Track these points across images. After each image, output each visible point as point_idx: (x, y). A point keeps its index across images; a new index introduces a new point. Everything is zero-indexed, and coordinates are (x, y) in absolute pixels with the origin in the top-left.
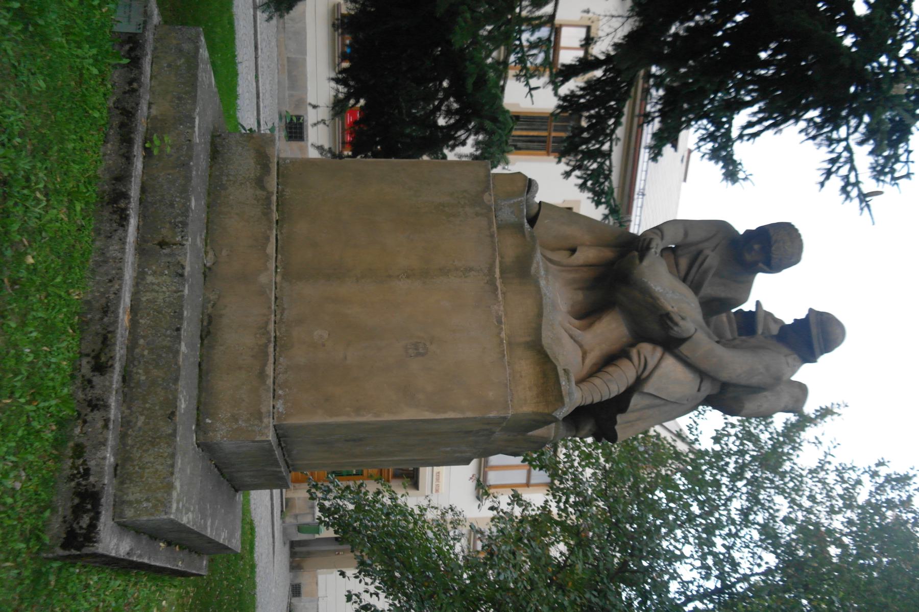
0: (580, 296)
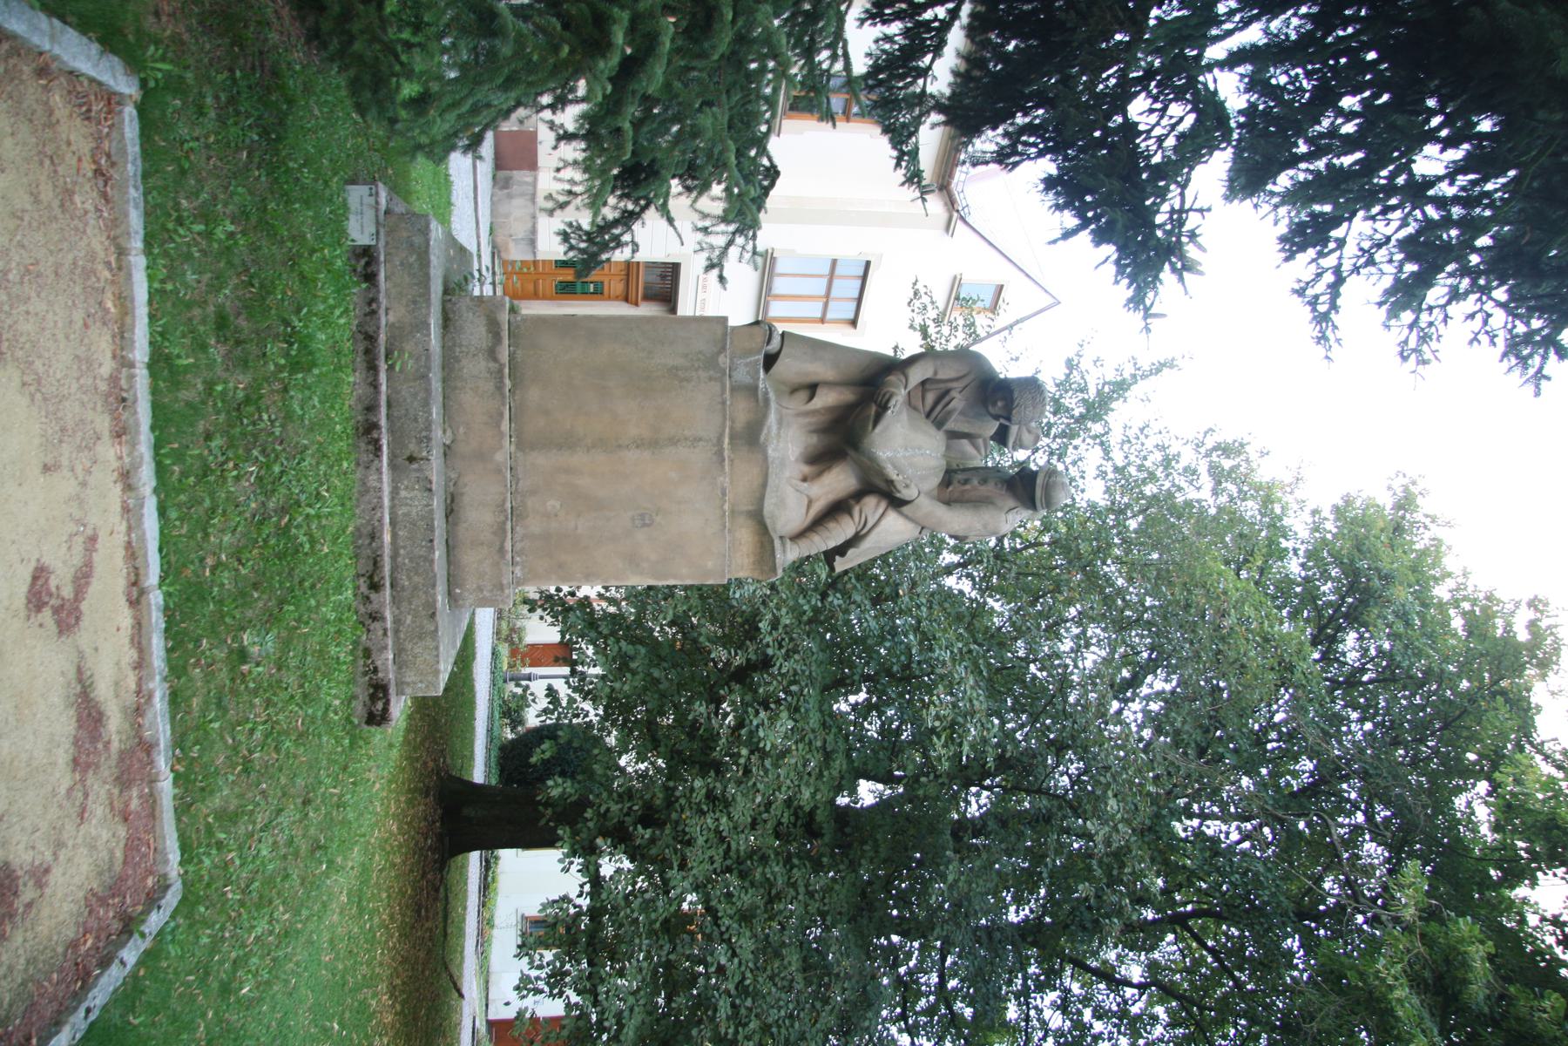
0: (814, 439)
